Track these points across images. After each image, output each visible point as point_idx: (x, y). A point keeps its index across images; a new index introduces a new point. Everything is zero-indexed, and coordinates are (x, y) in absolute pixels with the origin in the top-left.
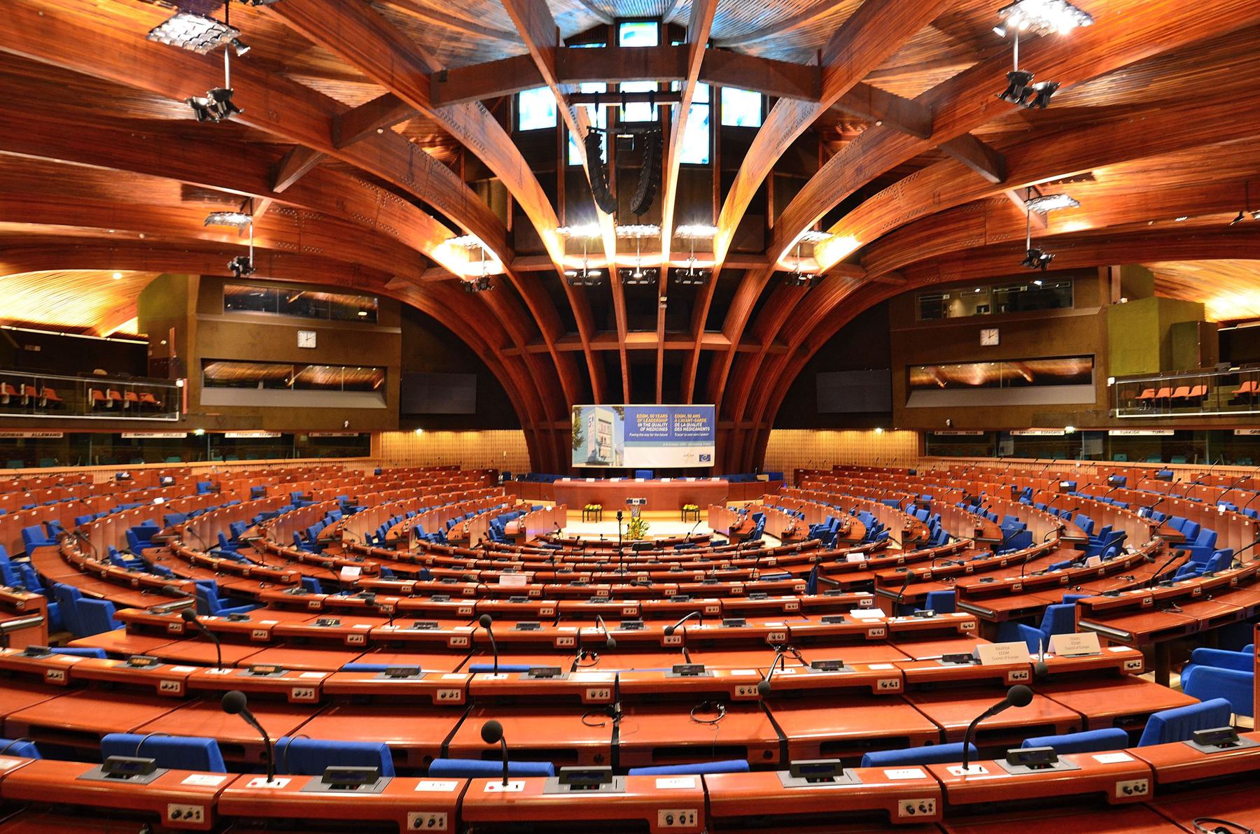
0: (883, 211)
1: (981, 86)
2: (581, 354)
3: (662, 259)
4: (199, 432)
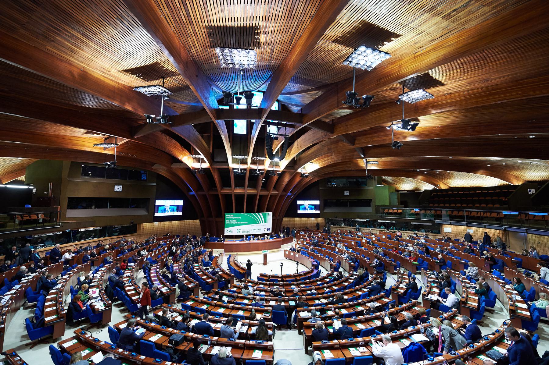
0: (328, 158)
1: (371, 136)
2: (217, 196)
3: (249, 166)
4: (68, 231)
